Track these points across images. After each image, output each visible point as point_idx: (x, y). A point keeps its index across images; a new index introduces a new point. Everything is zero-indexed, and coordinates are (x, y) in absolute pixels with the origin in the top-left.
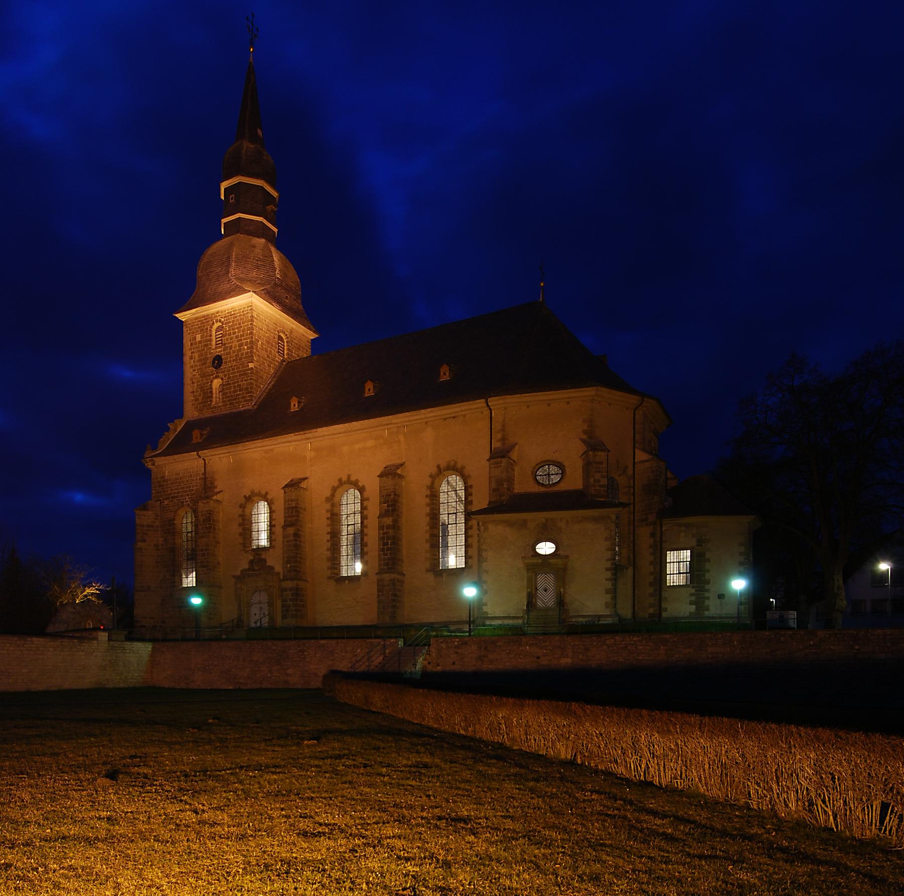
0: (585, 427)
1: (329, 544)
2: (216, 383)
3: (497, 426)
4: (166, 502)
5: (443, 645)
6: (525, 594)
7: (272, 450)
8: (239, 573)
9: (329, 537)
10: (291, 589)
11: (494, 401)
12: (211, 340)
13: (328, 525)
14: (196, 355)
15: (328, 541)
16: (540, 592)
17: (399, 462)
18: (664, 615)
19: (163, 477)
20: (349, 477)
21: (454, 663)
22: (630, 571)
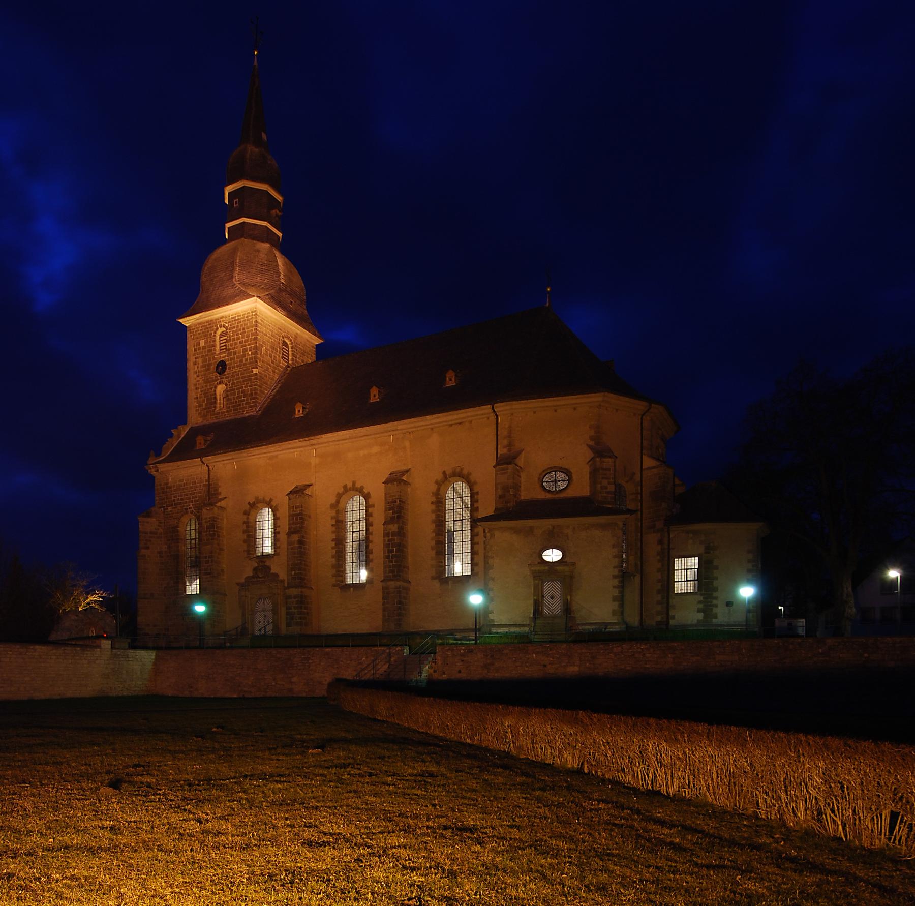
2: (220, 389)
3: (503, 432)
6: (531, 602)
7: (276, 456)
8: (243, 581)
11: (499, 407)
12: (214, 346)
13: (333, 532)
14: (200, 361)
15: (333, 548)
16: (547, 600)
17: (404, 468)
18: (672, 622)
19: (167, 484)
20: (354, 483)
22: (637, 579)
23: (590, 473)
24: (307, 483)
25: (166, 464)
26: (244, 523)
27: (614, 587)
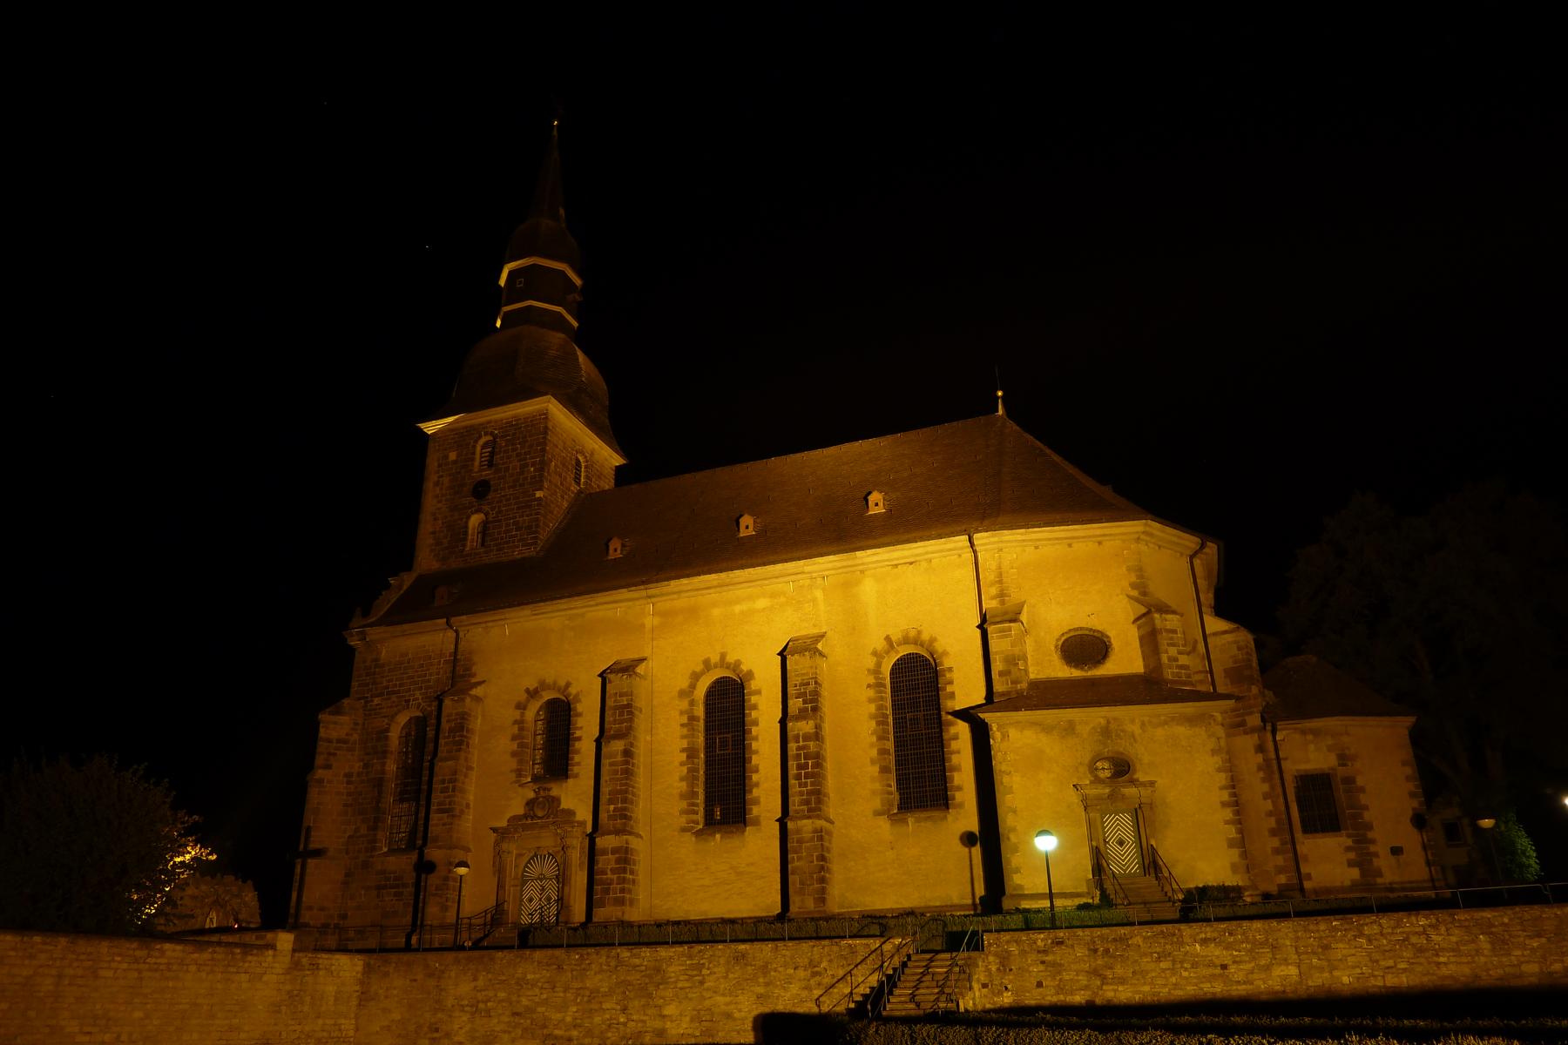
0: (1133, 579)
1: (685, 769)
2: (475, 520)
3: (987, 576)
4: (376, 701)
5: (1013, 948)
7: (583, 615)
8: (504, 824)
9: (684, 756)
10: (615, 851)
11: (981, 538)
12: (473, 460)
13: (683, 737)
14: (446, 480)
15: (682, 764)
16: (1113, 849)
17: (815, 631)
18: (1307, 885)
19: (377, 660)
20: (723, 656)
21: (1040, 985)
23: (1141, 639)
24: (636, 656)
25: (383, 629)
26: (516, 722)
27: (1227, 822)
